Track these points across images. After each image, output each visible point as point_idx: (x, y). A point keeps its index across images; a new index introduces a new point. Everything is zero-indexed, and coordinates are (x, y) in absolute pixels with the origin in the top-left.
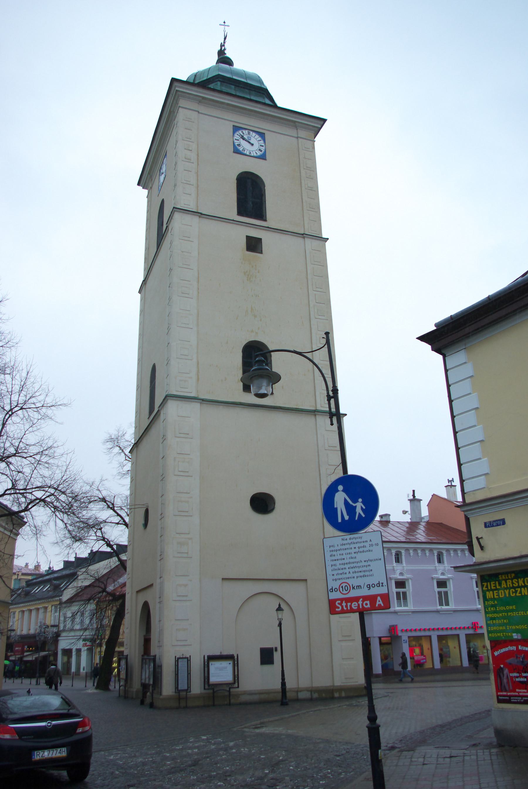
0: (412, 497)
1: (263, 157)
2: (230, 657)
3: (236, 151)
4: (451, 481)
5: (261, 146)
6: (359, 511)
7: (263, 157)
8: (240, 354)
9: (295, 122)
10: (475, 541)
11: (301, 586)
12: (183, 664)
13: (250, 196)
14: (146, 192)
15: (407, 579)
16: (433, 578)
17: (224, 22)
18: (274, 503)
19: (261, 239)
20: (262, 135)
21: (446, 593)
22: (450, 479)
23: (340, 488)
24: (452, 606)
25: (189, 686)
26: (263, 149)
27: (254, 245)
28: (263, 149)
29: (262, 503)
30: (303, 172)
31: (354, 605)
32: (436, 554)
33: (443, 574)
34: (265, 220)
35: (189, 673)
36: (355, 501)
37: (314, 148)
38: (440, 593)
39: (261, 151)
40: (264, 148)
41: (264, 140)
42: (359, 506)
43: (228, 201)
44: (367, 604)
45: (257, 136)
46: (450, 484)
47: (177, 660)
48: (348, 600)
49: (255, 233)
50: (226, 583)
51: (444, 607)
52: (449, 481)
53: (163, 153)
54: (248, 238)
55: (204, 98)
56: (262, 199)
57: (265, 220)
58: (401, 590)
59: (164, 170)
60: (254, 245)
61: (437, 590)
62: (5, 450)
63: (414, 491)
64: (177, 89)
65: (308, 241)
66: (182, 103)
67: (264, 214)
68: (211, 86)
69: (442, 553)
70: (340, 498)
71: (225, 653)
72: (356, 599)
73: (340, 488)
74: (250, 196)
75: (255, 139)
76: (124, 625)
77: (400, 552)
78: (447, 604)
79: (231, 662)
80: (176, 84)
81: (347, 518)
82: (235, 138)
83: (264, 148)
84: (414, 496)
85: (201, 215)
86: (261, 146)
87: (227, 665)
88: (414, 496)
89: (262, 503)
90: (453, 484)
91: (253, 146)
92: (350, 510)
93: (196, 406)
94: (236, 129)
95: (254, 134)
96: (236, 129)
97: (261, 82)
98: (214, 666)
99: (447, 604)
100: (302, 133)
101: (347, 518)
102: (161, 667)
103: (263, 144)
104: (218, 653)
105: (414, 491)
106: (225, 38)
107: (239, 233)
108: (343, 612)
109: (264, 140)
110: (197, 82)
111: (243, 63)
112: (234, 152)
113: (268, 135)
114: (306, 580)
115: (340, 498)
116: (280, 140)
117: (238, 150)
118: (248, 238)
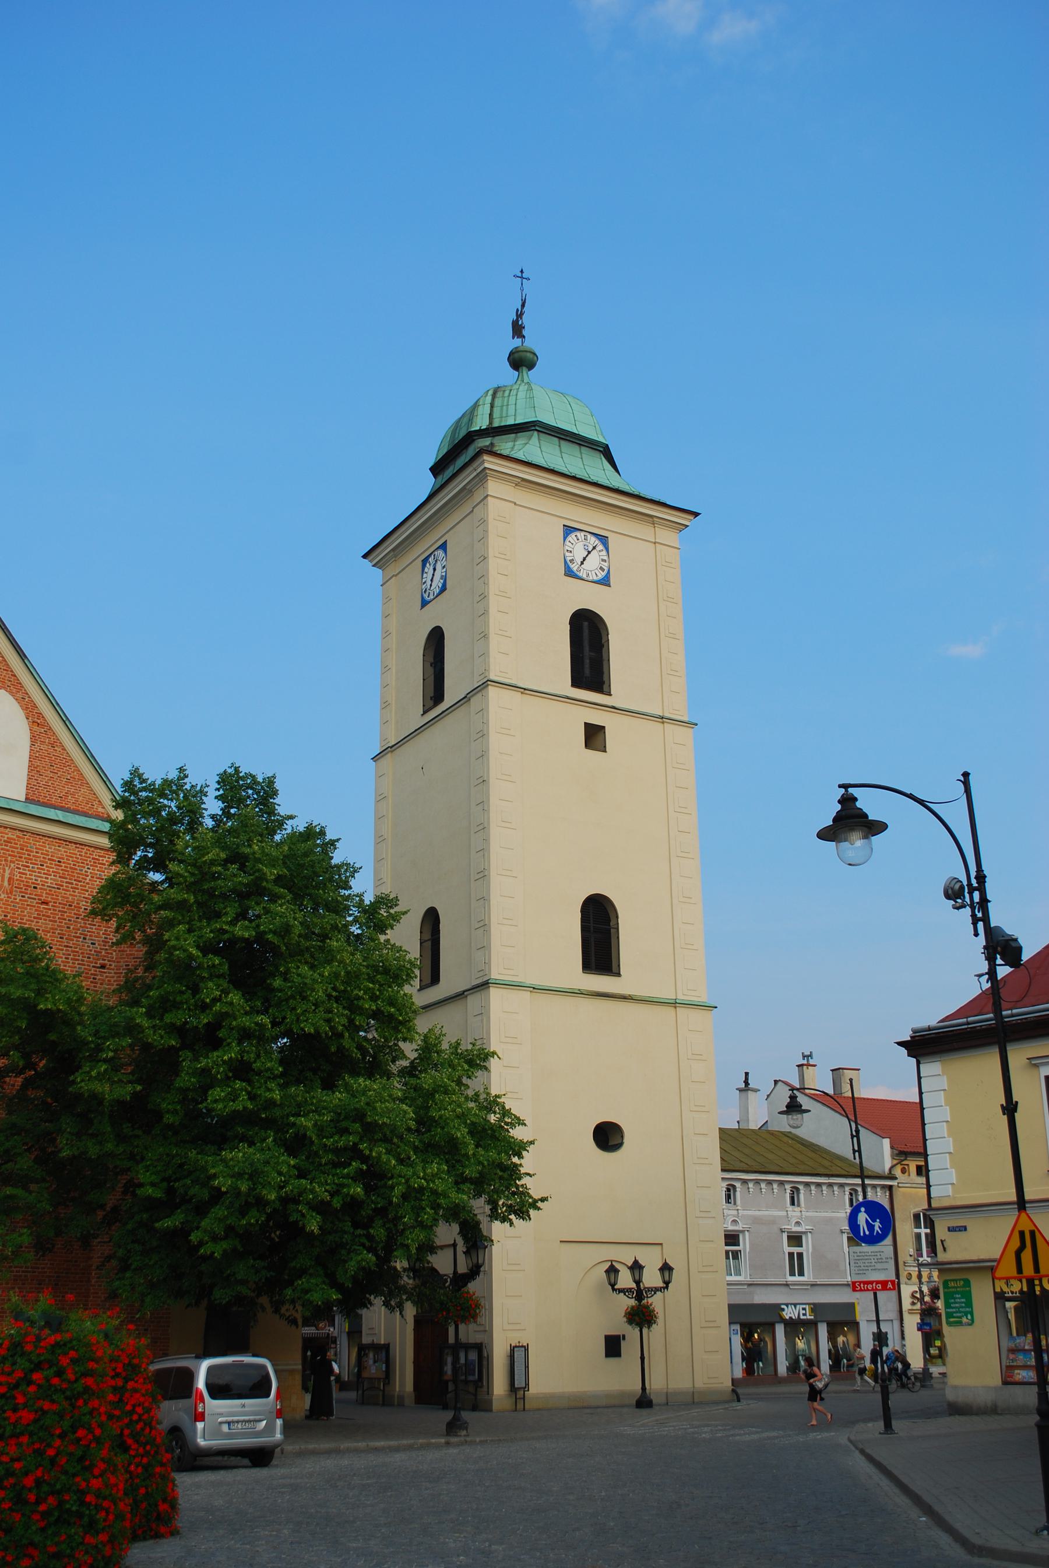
0: (743, 1085)
1: (605, 582)
3: (569, 573)
4: (808, 1056)
5: (603, 560)
6: (877, 1228)
7: (605, 582)
10: (938, 1243)
12: (519, 1354)
15: (743, 1232)
16: (782, 1231)
17: (522, 272)
18: (622, 1137)
19: (604, 727)
20: (604, 540)
21: (800, 1255)
23: (863, 1209)
25: (527, 1384)
26: (605, 565)
27: (594, 736)
28: (605, 565)
29: (607, 1136)
31: (870, 1287)
32: (788, 1191)
33: (798, 1223)
36: (874, 1221)
38: (791, 1255)
39: (602, 569)
40: (606, 564)
42: (877, 1225)
44: (880, 1286)
46: (805, 1062)
47: (513, 1349)
48: (865, 1283)
49: (596, 718)
50: (563, 1244)
51: (797, 1278)
52: (804, 1057)
60: (594, 736)
61: (787, 1249)
63: (747, 1074)
64: (487, 465)
66: (493, 487)
67: (605, 679)
69: (798, 1189)
70: (862, 1217)
72: (871, 1282)
73: (863, 1209)
77: (734, 1187)
81: (867, 1233)
82: (567, 548)
83: (606, 564)
84: (746, 1083)
86: (603, 560)
88: (746, 1083)
89: (607, 1136)
90: (811, 1062)
92: (870, 1227)
93: (526, 995)
94: (568, 530)
96: (568, 530)
101: (867, 1233)
103: (605, 558)
105: (747, 1074)
106: (523, 305)
107: (574, 719)
108: (861, 1290)
112: (566, 574)
115: (862, 1217)
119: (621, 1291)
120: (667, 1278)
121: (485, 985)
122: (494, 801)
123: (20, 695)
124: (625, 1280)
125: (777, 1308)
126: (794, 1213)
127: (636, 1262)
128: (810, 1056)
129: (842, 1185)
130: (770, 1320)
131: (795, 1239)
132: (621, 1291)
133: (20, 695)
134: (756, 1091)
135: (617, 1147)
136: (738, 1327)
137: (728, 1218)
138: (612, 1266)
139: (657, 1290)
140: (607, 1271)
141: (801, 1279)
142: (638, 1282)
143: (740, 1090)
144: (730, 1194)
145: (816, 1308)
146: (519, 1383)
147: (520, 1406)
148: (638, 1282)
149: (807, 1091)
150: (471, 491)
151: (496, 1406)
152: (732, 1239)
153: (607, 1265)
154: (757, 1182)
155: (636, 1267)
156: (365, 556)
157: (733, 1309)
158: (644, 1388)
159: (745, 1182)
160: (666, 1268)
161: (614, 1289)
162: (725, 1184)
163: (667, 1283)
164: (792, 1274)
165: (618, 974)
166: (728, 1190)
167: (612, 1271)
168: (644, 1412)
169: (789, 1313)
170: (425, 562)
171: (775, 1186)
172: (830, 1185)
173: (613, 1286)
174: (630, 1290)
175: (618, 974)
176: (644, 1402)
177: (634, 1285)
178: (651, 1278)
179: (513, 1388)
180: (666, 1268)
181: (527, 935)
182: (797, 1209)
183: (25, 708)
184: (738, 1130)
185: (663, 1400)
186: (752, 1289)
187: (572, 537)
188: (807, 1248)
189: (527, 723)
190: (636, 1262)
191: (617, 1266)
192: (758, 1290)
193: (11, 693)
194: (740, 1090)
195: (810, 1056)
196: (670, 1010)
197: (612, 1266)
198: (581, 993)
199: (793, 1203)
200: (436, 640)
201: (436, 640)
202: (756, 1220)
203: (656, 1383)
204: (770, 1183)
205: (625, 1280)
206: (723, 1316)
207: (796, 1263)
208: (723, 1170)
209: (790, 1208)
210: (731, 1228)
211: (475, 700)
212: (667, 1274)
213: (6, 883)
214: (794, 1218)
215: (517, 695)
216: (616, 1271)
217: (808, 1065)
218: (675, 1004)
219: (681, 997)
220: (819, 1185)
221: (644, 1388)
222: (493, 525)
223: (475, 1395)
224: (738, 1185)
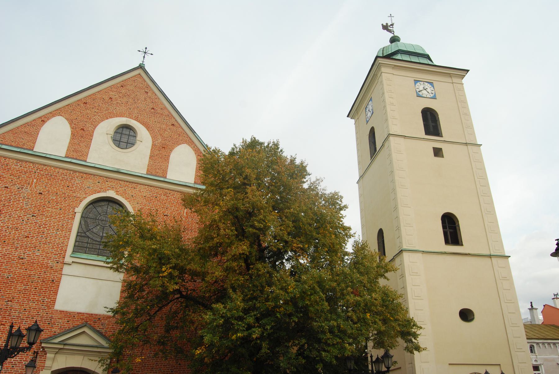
3: (418, 96)
7: (434, 98)
9: (449, 74)
13: (431, 121)
14: (353, 120)
15: (540, 365)
18: (474, 315)
20: (431, 84)
22: (556, 294)
26: (433, 92)
27: (438, 152)
29: (466, 315)
34: (442, 136)
37: (463, 88)
41: (433, 87)
43: (418, 126)
45: (429, 85)
49: (438, 145)
52: (555, 295)
53: (368, 99)
55: (395, 66)
59: (370, 107)
60: (438, 152)
63: (531, 303)
66: (383, 69)
68: (394, 57)
74: (431, 121)
75: (428, 86)
77: (533, 346)
80: (379, 59)
84: (532, 306)
85: (405, 137)
88: (532, 306)
89: (466, 315)
91: (427, 90)
93: (420, 255)
95: (427, 84)
96: (416, 81)
97: (423, 50)
100: (455, 80)
105: (531, 303)
109: (433, 87)
110: (385, 55)
111: (408, 40)
113: (435, 84)
114: (500, 365)
116: (443, 85)
117: (419, 95)
121: (401, 252)
122: (397, 178)
123: (193, 146)
133: (193, 146)
137: (533, 359)
143: (529, 309)
144: (532, 349)
150: (377, 75)
154: (543, 343)
156: (348, 116)
159: (538, 344)
162: (529, 345)
165: (462, 245)
166: (531, 347)
170: (366, 109)
171: (552, 345)
175: (462, 245)
181: (419, 230)
183: (195, 150)
184: (531, 325)
187: (418, 84)
193: (189, 145)
195: (557, 294)
196: (488, 260)
198: (445, 253)
200: (372, 132)
201: (372, 132)
202: (546, 360)
204: (549, 344)
208: (527, 339)
210: (535, 363)
211: (386, 145)
213: (185, 214)
215: (402, 139)
218: (490, 256)
224: (535, 345)
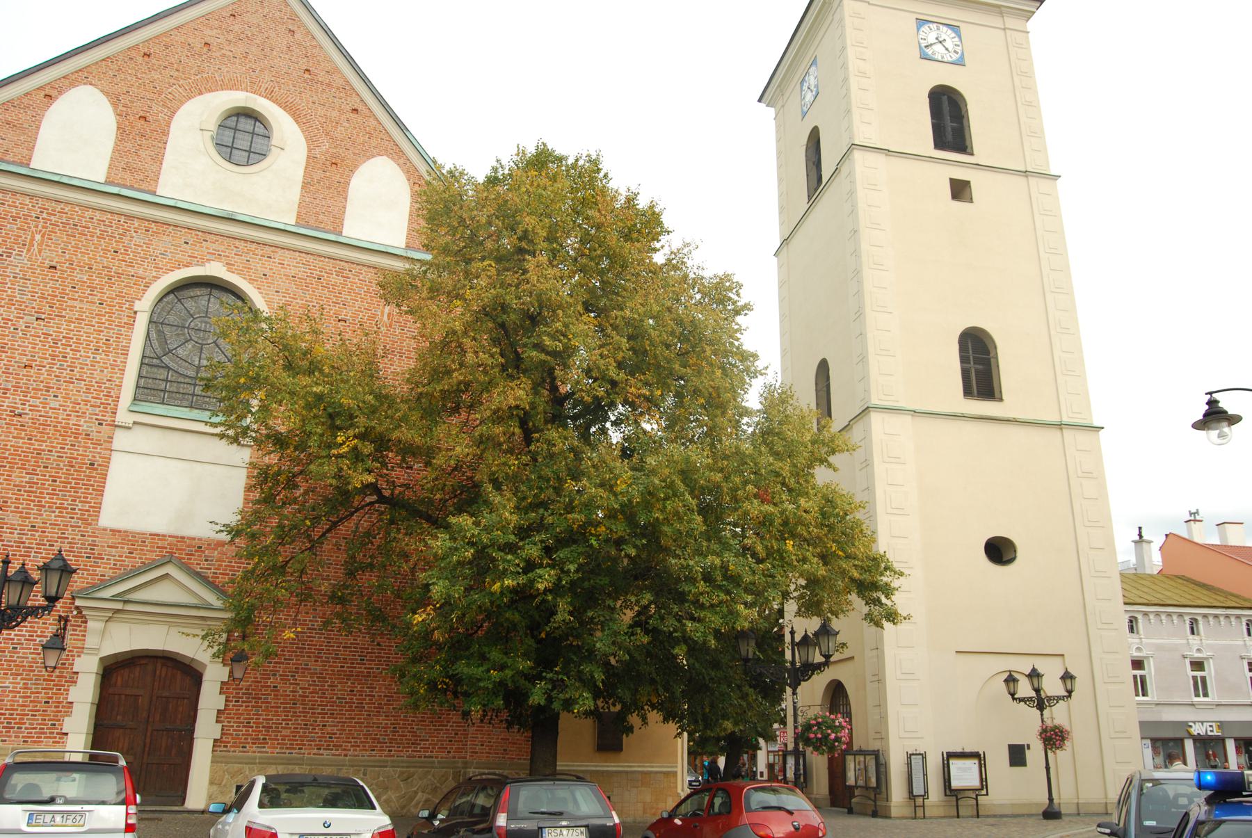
2: (975, 755)
3: (925, 57)
7: (960, 63)
8: (957, 347)
11: (1059, 659)
12: (916, 761)
13: (949, 119)
15: (1147, 657)
16: (1184, 657)
19: (968, 183)
20: (955, 28)
21: (1204, 679)
24: (1213, 697)
25: (926, 792)
26: (959, 49)
27: (960, 190)
28: (959, 49)
29: (999, 551)
30: (1016, 79)
32: (1188, 622)
33: (1198, 650)
35: (925, 775)
38: (1194, 678)
41: (960, 37)
43: (919, 127)
45: (950, 32)
47: (910, 756)
49: (961, 174)
51: (1202, 699)
54: (952, 181)
56: (962, 123)
57: (972, 154)
58: (1138, 673)
60: (960, 190)
62: (301, 472)
65: (1033, 181)
67: (968, 143)
69: (1196, 620)
71: (967, 750)
74: (949, 119)
75: (946, 34)
76: (58, 780)
78: (1206, 695)
79: (976, 761)
84: (1140, 535)
85: (888, 152)
87: (972, 764)
88: (1140, 535)
89: (999, 551)
91: (943, 42)
93: (908, 419)
95: (945, 29)
96: (921, 22)
98: (955, 764)
99: (1206, 695)
100: (1011, 22)
102: (886, 765)
104: (960, 750)
109: (960, 37)
118: (952, 181)
119: (1021, 700)
120: (1069, 687)
123: (401, 161)
124: (1025, 689)
125: (1185, 725)
126: (1194, 640)
127: (1034, 670)
128: (1197, 512)
129: (1238, 617)
130: (1178, 735)
131: (1198, 665)
132: (1021, 700)
133: (401, 161)
134: (1150, 542)
135: (1011, 561)
136: (1148, 742)
137: (1132, 646)
138: (1010, 676)
139: (1059, 698)
140: (1006, 681)
141: (1206, 699)
142: (1037, 691)
143: (1135, 542)
144: (1132, 625)
145: (1221, 725)
146: (918, 790)
147: (920, 813)
148: (1037, 691)
149: (1108, 831)
151: (894, 813)
152: (1138, 664)
153: (1005, 676)
154: (1157, 614)
155: (1034, 675)
156: (760, 100)
157: (1143, 724)
158: (1051, 799)
159: (1146, 614)
160: (1067, 677)
161: (1014, 699)
163: (1070, 692)
164: (1197, 695)
165: (1001, 400)
166: (1131, 621)
167: (1011, 680)
168: (1052, 823)
169: (1197, 730)
170: (802, 83)
172: (1227, 617)
173: (1013, 695)
174: (1030, 699)
176: (1051, 814)
177: (1033, 694)
178: (1052, 686)
179: (911, 796)
180: (1067, 677)
182: (1195, 637)
183: (407, 172)
184: (1135, 574)
185: (1073, 810)
186: (1160, 708)
187: (925, 28)
188: (1210, 672)
189: (894, 184)
190: (1034, 670)
191: (1016, 676)
192: (1166, 709)
193: (393, 159)
194: (1135, 542)
195: (1197, 512)
197: (1010, 676)
199: (1193, 633)
202: (1159, 648)
203: (1065, 796)
204: (1169, 615)
205: (1025, 689)
206: (1137, 733)
207: (1201, 687)
208: (1126, 604)
209: (1191, 637)
210: (1135, 654)
211: (845, 170)
212: (1068, 682)
214: (1195, 646)
215: (881, 158)
216: (1015, 681)
217: (1195, 520)
218: (1060, 426)
219: (1066, 420)
220: (1216, 616)
221: (1051, 799)
222: (848, 21)
223: (875, 801)
